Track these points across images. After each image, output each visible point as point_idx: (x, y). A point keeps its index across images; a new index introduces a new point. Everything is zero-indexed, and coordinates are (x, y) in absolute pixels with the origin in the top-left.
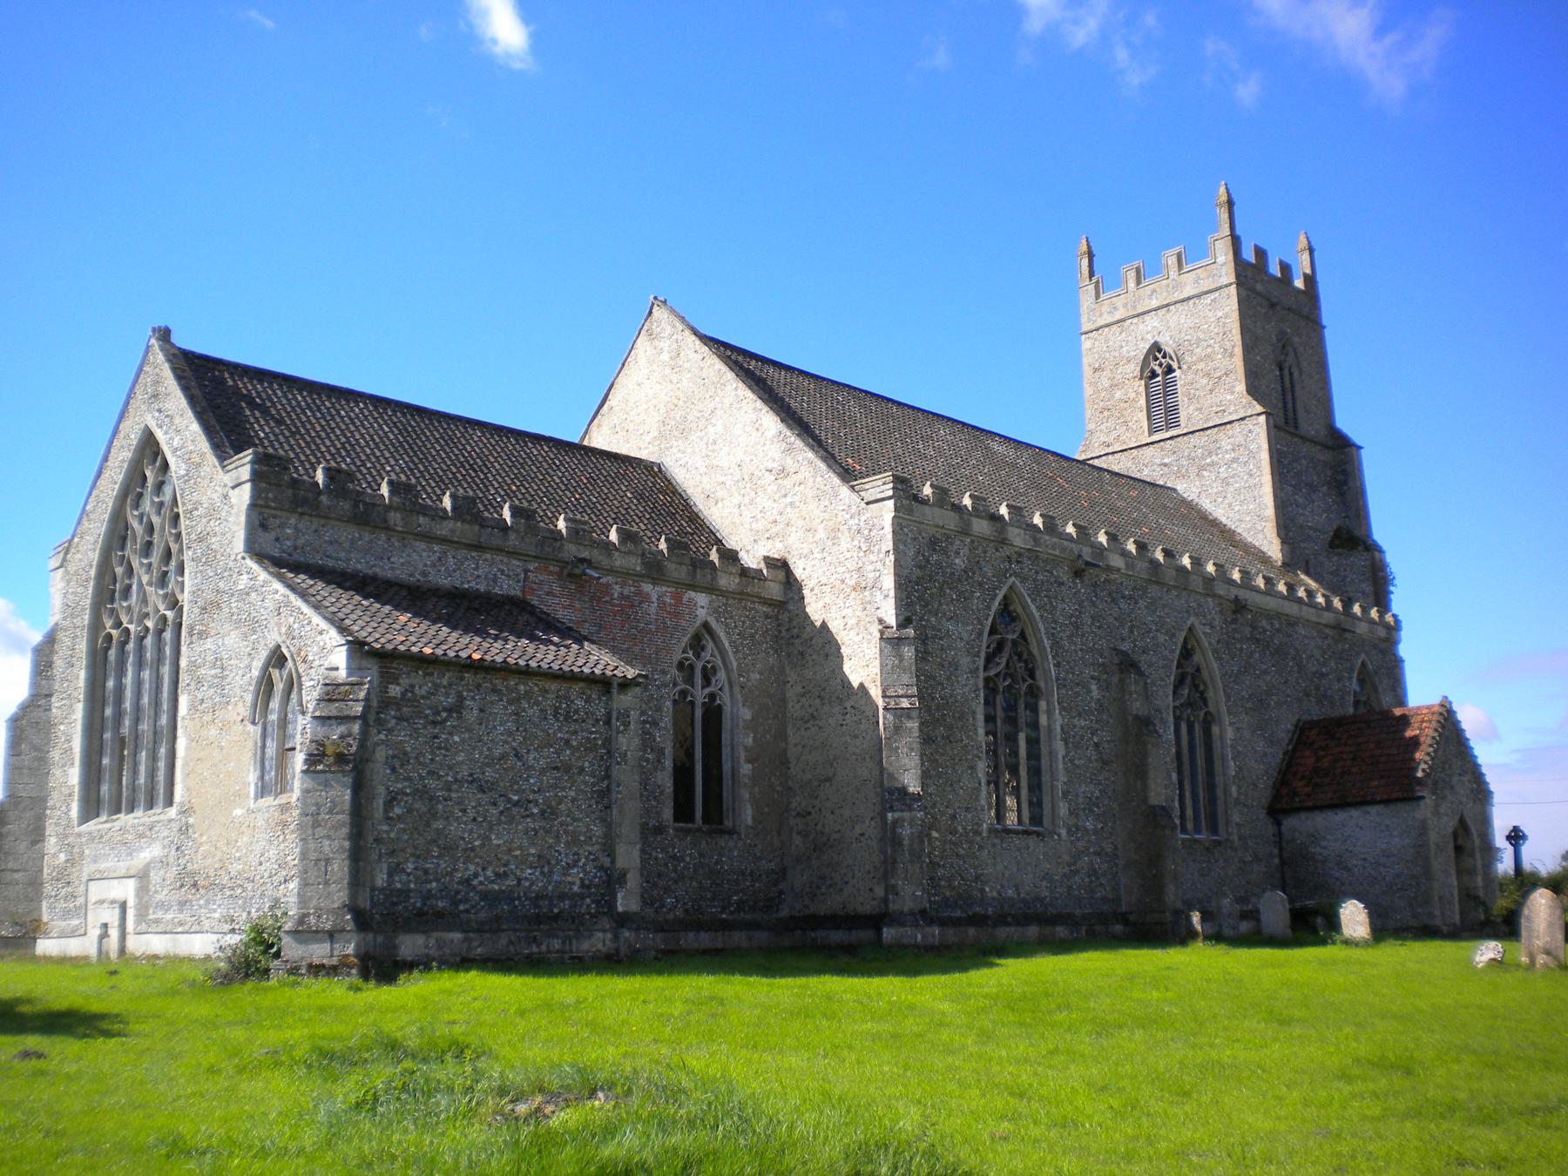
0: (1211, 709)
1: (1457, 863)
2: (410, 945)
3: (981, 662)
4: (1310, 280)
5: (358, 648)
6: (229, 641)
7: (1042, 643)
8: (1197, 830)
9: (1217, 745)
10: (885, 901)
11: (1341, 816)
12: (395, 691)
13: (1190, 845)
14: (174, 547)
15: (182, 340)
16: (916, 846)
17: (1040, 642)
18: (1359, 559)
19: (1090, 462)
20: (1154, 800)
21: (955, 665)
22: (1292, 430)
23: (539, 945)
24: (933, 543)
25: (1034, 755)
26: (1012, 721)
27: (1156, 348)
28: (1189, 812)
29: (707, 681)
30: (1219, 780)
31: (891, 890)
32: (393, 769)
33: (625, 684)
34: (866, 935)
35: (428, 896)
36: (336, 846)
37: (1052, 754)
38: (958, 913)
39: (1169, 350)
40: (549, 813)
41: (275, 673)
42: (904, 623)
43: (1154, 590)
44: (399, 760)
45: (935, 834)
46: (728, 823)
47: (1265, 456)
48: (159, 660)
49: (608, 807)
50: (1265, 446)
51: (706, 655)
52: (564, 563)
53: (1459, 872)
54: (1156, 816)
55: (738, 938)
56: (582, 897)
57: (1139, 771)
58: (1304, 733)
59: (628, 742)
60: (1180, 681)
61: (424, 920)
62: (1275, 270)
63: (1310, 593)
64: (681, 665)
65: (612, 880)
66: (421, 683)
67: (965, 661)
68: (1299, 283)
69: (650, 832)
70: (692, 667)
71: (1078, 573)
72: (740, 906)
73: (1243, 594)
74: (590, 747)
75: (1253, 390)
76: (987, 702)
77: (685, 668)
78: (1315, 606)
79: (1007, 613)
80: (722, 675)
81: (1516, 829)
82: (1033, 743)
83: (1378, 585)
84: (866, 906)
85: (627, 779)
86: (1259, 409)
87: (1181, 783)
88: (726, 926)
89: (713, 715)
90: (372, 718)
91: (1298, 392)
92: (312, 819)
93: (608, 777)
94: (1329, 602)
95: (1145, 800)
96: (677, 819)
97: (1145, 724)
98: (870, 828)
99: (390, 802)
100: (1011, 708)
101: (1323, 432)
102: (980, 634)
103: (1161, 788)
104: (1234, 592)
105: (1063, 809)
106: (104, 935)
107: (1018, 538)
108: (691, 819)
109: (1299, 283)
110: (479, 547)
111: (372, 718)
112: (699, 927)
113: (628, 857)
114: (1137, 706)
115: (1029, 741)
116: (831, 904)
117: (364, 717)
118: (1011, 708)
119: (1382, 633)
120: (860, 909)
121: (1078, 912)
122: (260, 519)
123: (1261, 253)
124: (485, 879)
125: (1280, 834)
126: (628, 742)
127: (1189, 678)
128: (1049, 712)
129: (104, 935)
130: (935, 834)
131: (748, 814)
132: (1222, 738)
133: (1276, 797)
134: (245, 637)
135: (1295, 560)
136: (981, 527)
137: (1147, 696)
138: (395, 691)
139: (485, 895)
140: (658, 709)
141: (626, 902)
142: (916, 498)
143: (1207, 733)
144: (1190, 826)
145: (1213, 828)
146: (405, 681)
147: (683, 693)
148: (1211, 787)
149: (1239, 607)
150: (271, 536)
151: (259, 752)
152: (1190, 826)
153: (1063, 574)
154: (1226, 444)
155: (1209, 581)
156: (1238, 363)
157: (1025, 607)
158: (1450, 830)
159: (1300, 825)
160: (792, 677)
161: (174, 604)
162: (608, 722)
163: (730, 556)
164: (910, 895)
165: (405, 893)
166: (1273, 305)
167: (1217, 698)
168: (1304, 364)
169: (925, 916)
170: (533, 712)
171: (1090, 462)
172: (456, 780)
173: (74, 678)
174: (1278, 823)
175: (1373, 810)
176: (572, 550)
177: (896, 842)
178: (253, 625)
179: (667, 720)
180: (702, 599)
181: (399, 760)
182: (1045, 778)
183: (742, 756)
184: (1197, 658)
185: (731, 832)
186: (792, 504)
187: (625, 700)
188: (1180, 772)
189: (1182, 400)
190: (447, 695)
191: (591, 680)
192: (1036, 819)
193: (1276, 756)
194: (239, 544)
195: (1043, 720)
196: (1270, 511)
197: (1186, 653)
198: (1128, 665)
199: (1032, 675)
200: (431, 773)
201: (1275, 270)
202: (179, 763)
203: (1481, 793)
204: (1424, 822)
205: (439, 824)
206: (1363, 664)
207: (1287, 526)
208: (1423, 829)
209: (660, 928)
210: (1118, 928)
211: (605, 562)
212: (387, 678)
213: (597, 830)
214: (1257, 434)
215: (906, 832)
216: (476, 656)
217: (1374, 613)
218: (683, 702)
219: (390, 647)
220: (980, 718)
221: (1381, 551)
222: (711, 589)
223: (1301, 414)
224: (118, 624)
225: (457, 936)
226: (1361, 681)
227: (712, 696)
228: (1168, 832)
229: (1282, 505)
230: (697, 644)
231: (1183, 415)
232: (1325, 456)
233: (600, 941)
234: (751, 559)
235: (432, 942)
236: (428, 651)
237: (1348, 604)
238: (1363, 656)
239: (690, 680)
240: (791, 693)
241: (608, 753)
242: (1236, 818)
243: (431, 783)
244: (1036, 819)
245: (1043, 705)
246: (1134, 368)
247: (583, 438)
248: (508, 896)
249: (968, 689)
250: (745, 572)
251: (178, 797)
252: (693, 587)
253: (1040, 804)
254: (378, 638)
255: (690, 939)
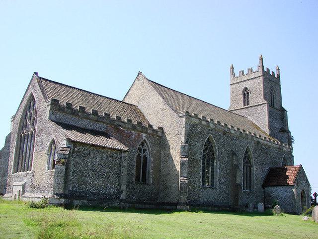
2: (76, 202)
3: (202, 151)
4: (278, 76)
5: (69, 140)
6: (44, 136)
7: (216, 149)
8: (247, 189)
9: (252, 171)
10: (178, 200)
11: (277, 188)
12: (76, 149)
15: (40, 75)
18: (286, 135)
19: (235, 112)
24: (194, 126)
26: (208, 164)
27: (246, 89)
29: (144, 152)
30: (252, 179)
31: (180, 198)
33: (125, 151)
34: (174, 207)
35: (80, 193)
36: (61, 181)
37: (217, 171)
40: (107, 177)
42: (186, 142)
44: (76, 163)
47: (267, 112)
48: (31, 141)
50: (267, 110)
52: (115, 126)
56: (113, 195)
57: (235, 176)
59: (125, 164)
60: (245, 158)
61: (79, 197)
62: (271, 73)
63: (265, 138)
64: (139, 149)
67: (199, 151)
68: (276, 76)
69: (129, 183)
72: (148, 199)
73: (259, 140)
75: (265, 98)
76: (203, 160)
77: (140, 149)
78: (275, 144)
79: (209, 141)
80: (148, 151)
81: (316, 193)
82: (213, 169)
83: (290, 141)
84: (175, 201)
85: (124, 171)
86: (266, 102)
87: (244, 179)
88: (145, 204)
89: (145, 159)
90: (71, 155)
92: (57, 175)
94: (278, 143)
99: (74, 172)
100: (208, 162)
103: (240, 179)
104: (258, 140)
107: (212, 126)
109: (276, 76)
110: (98, 121)
111: (71, 155)
112: (140, 203)
113: (124, 187)
114: (235, 163)
115: (212, 168)
116: (168, 200)
117: (69, 154)
118: (208, 162)
119: (289, 150)
122: (52, 113)
123: (268, 69)
124: (93, 190)
126: (125, 164)
127: (247, 158)
128: (216, 163)
131: (151, 181)
132: (253, 170)
135: (273, 135)
136: (204, 123)
139: (93, 193)
142: (191, 116)
143: (250, 169)
144: (245, 188)
145: (250, 189)
146: (78, 148)
147: (139, 154)
148: (250, 180)
149: (258, 143)
150: (54, 116)
152: (245, 188)
153: (221, 134)
155: (252, 136)
156: (262, 92)
157: (213, 140)
158: (300, 192)
159: (269, 189)
160: (162, 152)
161: (34, 129)
162: (121, 159)
163: (151, 126)
165: (75, 192)
167: (253, 162)
171: (235, 112)
173: (14, 144)
174: (264, 189)
176: (117, 123)
178: (48, 134)
179: (135, 159)
180: (144, 135)
181: (76, 163)
182: (215, 176)
184: (249, 153)
185: (148, 184)
187: (125, 155)
188: (244, 176)
189: (250, 99)
191: (118, 150)
192: (212, 185)
194: (48, 118)
195: (215, 164)
196: (267, 124)
197: (247, 152)
198: (234, 154)
199: (213, 155)
203: (308, 185)
206: (284, 157)
207: (271, 127)
209: (130, 203)
211: (124, 126)
212: (75, 146)
214: (266, 108)
216: (94, 143)
217: (287, 146)
218: (139, 157)
219: (75, 140)
220: (201, 163)
221: (290, 132)
222: (147, 133)
223: (275, 104)
224: (23, 133)
225: (86, 201)
226: (284, 160)
229: (270, 122)
230: (142, 144)
231: (250, 103)
232: (279, 113)
234: (155, 127)
236: (83, 142)
237: (282, 144)
239: (140, 151)
240: (162, 156)
241: (120, 166)
242: (255, 187)
244: (212, 185)
245: (215, 161)
246: (241, 92)
247: (124, 99)
249: (199, 156)
250: (153, 130)
253: (213, 182)
254: (73, 138)
255: (137, 206)
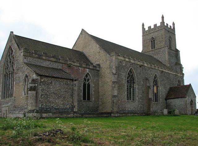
0: (158, 85)
1: (191, 106)
7: (135, 76)
10: (112, 110)
12: (42, 80)
13: (154, 104)
14: (13, 62)
16: (116, 103)
17: (135, 76)
20: (150, 97)
21: (123, 79)
22: (170, 48)
23: (63, 115)
25: (133, 91)
28: (154, 99)
32: (42, 91)
35: (47, 108)
38: (122, 112)
39: (154, 38)
40: (64, 98)
41: (26, 78)
43: (151, 69)
45: (119, 102)
46: (91, 100)
49: (73, 97)
51: (88, 77)
53: (191, 107)
54: (150, 100)
55: (91, 116)
57: (148, 93)
58: (171, 88)
59: (76, 88)
61: (47, 111)
62: (169, 27)
65: (73, 107)
66: (46, 79)
69: (79, 101)
70: (86, 79)
71: (140, 67)
74: (70, 89)
77: (85, 79)
84: (109, 111)
88: (90, 114)
89: (89, 85)
91: (172, 44)
93: (73, 93)
95: (148, 97)
96: (83, 100)
97: (149, 87)
98: (111, 101)
99: (41, 96)
101: (175, 49)
102: (126, 75)
105: (137, 98)
106: (4, 115)
108: (86, 100)
113: (76, 104)
114: (148, 85)
116: (104, 111)
120: (109, 112)
121: (138, 112)
124: (55, 106)
125: (166, 102)
126: (76, 88)
128: (136, 85)
129: (4, 115)
130: (119, 102)
131: (93, 99)
133: (166, 97)
134: (22, 73)
137: (150, 84)
138: (42, 80)
139: (55, 109)
140: (81, 85)
141: (75, 110)
146: (44, 79)
151: (4, 77)
152: (154, 101)
153: (138, 66)
154: (161, 50)
157: (133, 71)
159: (169, 101)
164: (115, 109)
166: (169, 32)
168: (173, 40)
169: (117, 112)
170: (62, 84)
172: (51, 93)
175: (179, 99)
177: (114, 102)
180: (88, 70)
183: (93, 91)
186: (101, 57)
190: (50, 81)
193: (167, 92)
195: (135, 86)
197: (155, 78)
200: (48, 92)
201: (169, 27)
202: (14, 91)
204: (186, 100)
205: (48, 99)
208: (186, 101)
210: (144, 114)
213: (71, 100)
215: (115, 101)
220: (126, 86)
223: (172, 47)
227: (89, 83)
228: (151, 101)
230: (87, 76)
232: (175, 52)
233: (72, 115)
235: (47, 115)
236: (47, 75)
238: (179, 79)
239: (85, 81)
241: (73, 90)
242: (161, 100)
243: (47, 93)
245: (135, 84)
248: (58, 109)
251: (14, 96)
252: (86, 68)
